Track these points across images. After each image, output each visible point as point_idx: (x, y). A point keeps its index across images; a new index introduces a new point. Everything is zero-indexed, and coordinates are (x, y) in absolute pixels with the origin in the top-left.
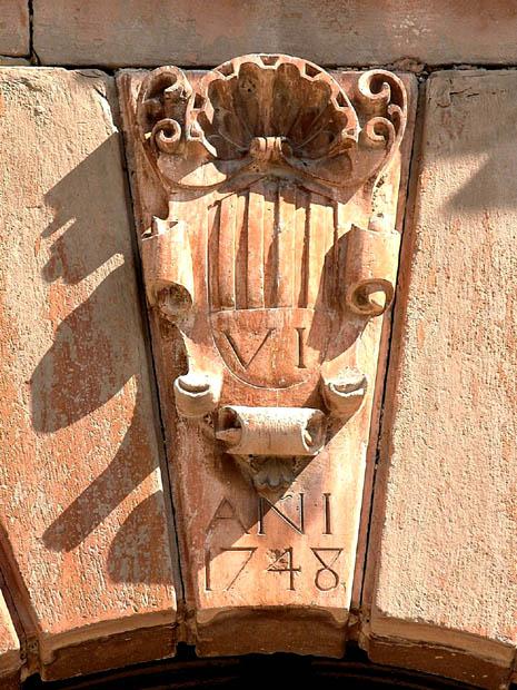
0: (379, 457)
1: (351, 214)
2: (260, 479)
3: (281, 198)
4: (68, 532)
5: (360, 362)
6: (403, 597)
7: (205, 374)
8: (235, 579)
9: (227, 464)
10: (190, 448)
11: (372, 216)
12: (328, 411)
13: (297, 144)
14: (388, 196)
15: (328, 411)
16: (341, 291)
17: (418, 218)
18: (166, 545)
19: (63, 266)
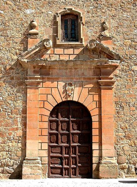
0: (73, 95)
1: (72, 87)
2: (69, 96)
3: (59, 114)
4: (63, 98)
5: (72, 92)
6: (74, 100)
7: (68, 93)
8: (69, 99)
9: (68, 95)
10: (67, 95)
11: (73, 87)
12: (72, 94)
13: (71, 85)
14: (74, 86)
15: (72, 94)
16: (72, 90)
17: (57, 48)
18: (66, 98)
19: (63, 89)
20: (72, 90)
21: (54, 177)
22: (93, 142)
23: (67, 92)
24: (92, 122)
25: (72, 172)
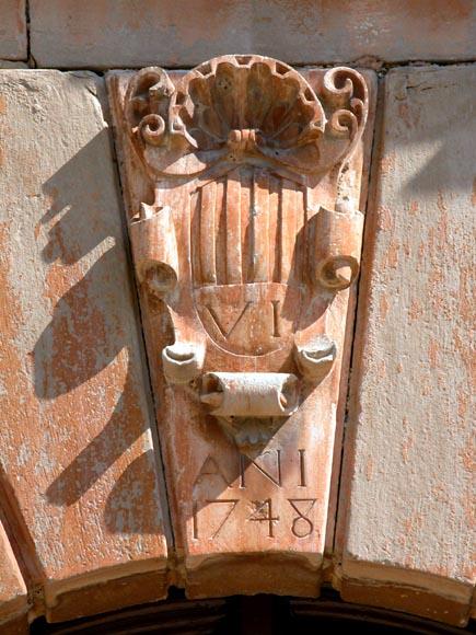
4: (68, 489)
5: (328, 333)
6: (372, 542)
7: (189, 344)
8: (220, 528)
9: (211, 424)
10: (178, 411)
11: (339, 199)
12: (302, 376)
14: (351, 182)
15: (302, 376)
16: (314, 268)
18: (158, 498)
19: (61, 248)
20: (314, 268)
21: (171, 499)
22: (317, 544)
23: (151, 343)
24: (83, 149)
25: (240, 234)
